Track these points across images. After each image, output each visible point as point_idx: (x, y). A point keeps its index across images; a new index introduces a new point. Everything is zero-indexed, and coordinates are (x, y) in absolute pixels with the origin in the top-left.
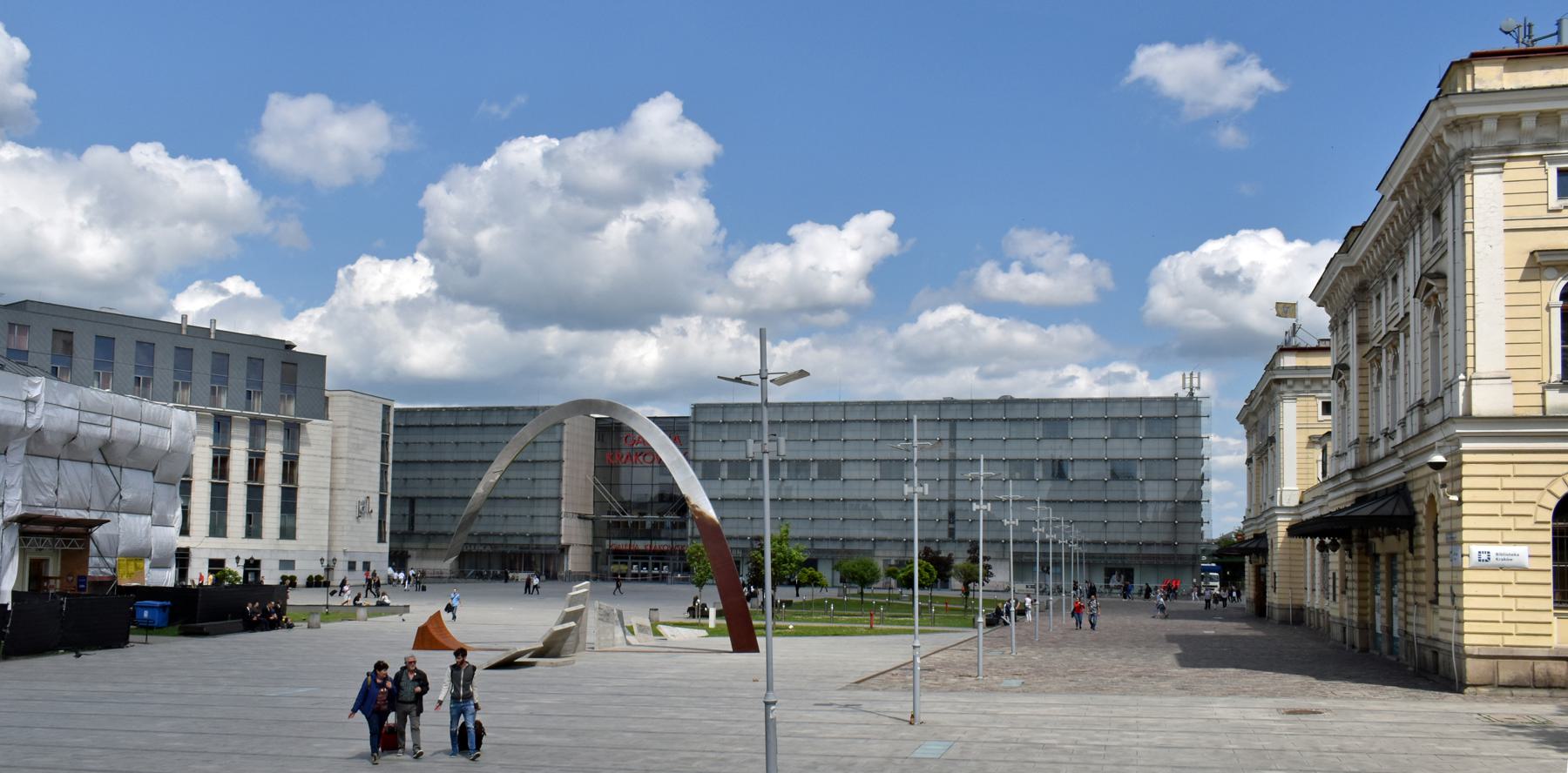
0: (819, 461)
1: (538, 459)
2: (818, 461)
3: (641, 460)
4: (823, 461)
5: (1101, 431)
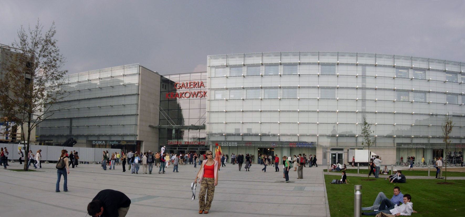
3: (184, 97)
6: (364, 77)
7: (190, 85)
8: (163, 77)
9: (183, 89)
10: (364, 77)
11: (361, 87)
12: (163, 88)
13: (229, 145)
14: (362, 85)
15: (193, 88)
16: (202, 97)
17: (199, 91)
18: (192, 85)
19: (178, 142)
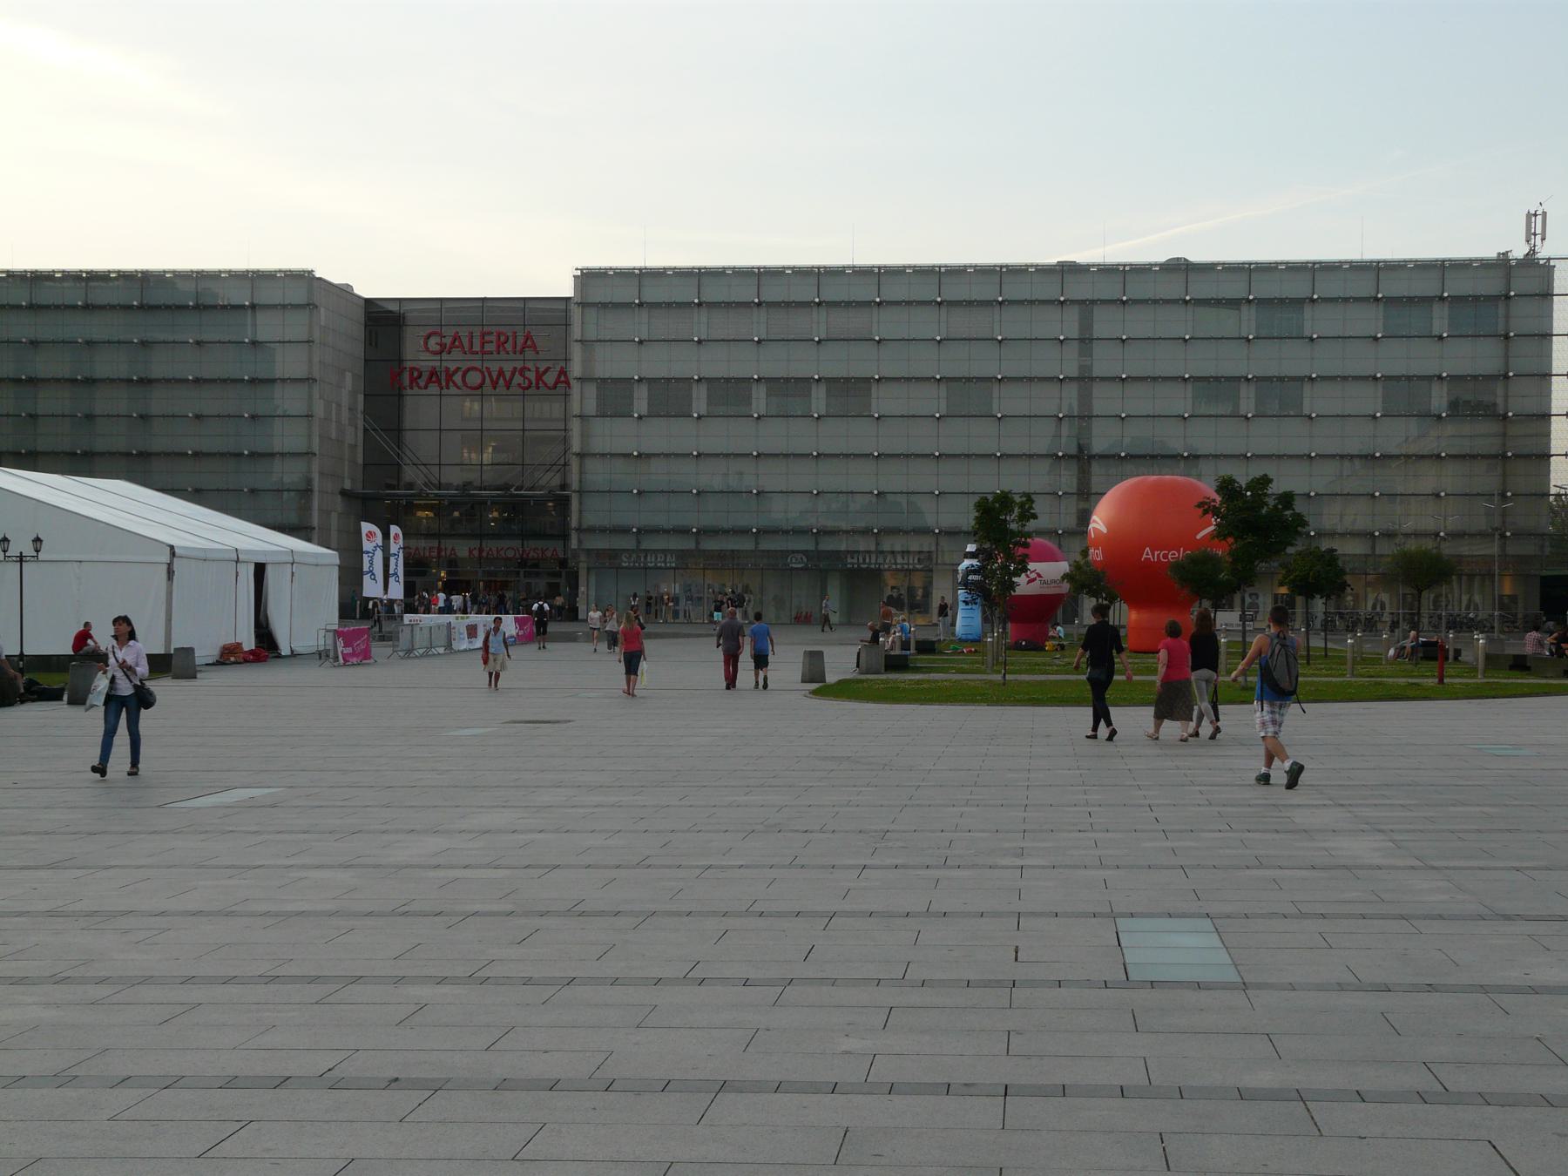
0: (709, 380)
1: (207, 376)
2: (707, 379)
3: (459, 382)
4: (718, 379)
5: (1369, 321)
6: (1086, 341)
7: (483, 343)
8: (377, 305)
9: (456, 354)
10: (1086, 341)
11: (1075, 374)
12: (371, 344)
13: (863, 566)
14: (1081, 367)
15: (495, 356)
16: (530, 386)
17: (519, 365)
18: (492, 342)
19: (439, 550)
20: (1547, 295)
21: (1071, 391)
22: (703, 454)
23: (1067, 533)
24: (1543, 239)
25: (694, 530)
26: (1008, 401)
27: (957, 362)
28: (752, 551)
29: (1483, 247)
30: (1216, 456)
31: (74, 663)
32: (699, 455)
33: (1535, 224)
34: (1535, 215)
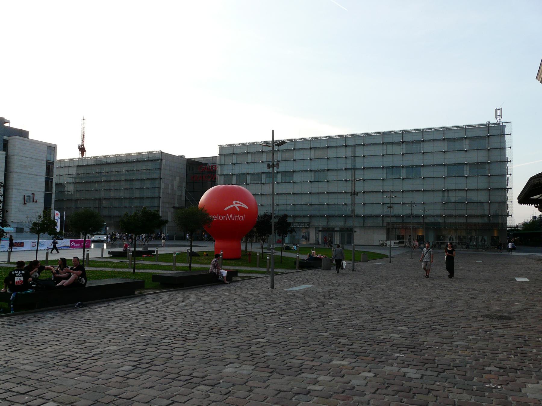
20: (503, 135)
21: (349, 173)
22: (404, 191)
23: (448, 216)
24: (501, 117)
25: (381, 216)
26: (331, 176)
27: (315, 166)
28: (443, 223)
29: (482, 120)
30: (455, 190)
31: (145, 255)
32: (403, 191)
33: (499, 112)
34: (499, 109)
